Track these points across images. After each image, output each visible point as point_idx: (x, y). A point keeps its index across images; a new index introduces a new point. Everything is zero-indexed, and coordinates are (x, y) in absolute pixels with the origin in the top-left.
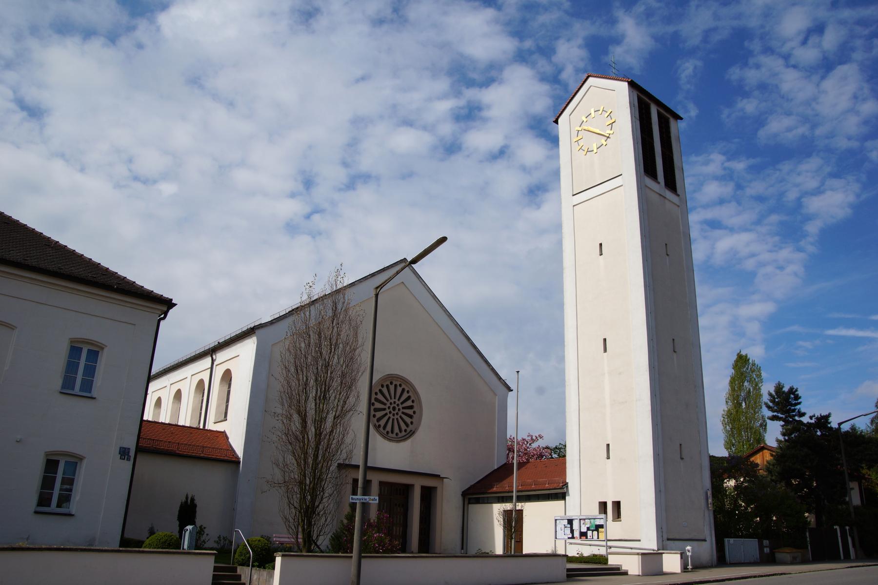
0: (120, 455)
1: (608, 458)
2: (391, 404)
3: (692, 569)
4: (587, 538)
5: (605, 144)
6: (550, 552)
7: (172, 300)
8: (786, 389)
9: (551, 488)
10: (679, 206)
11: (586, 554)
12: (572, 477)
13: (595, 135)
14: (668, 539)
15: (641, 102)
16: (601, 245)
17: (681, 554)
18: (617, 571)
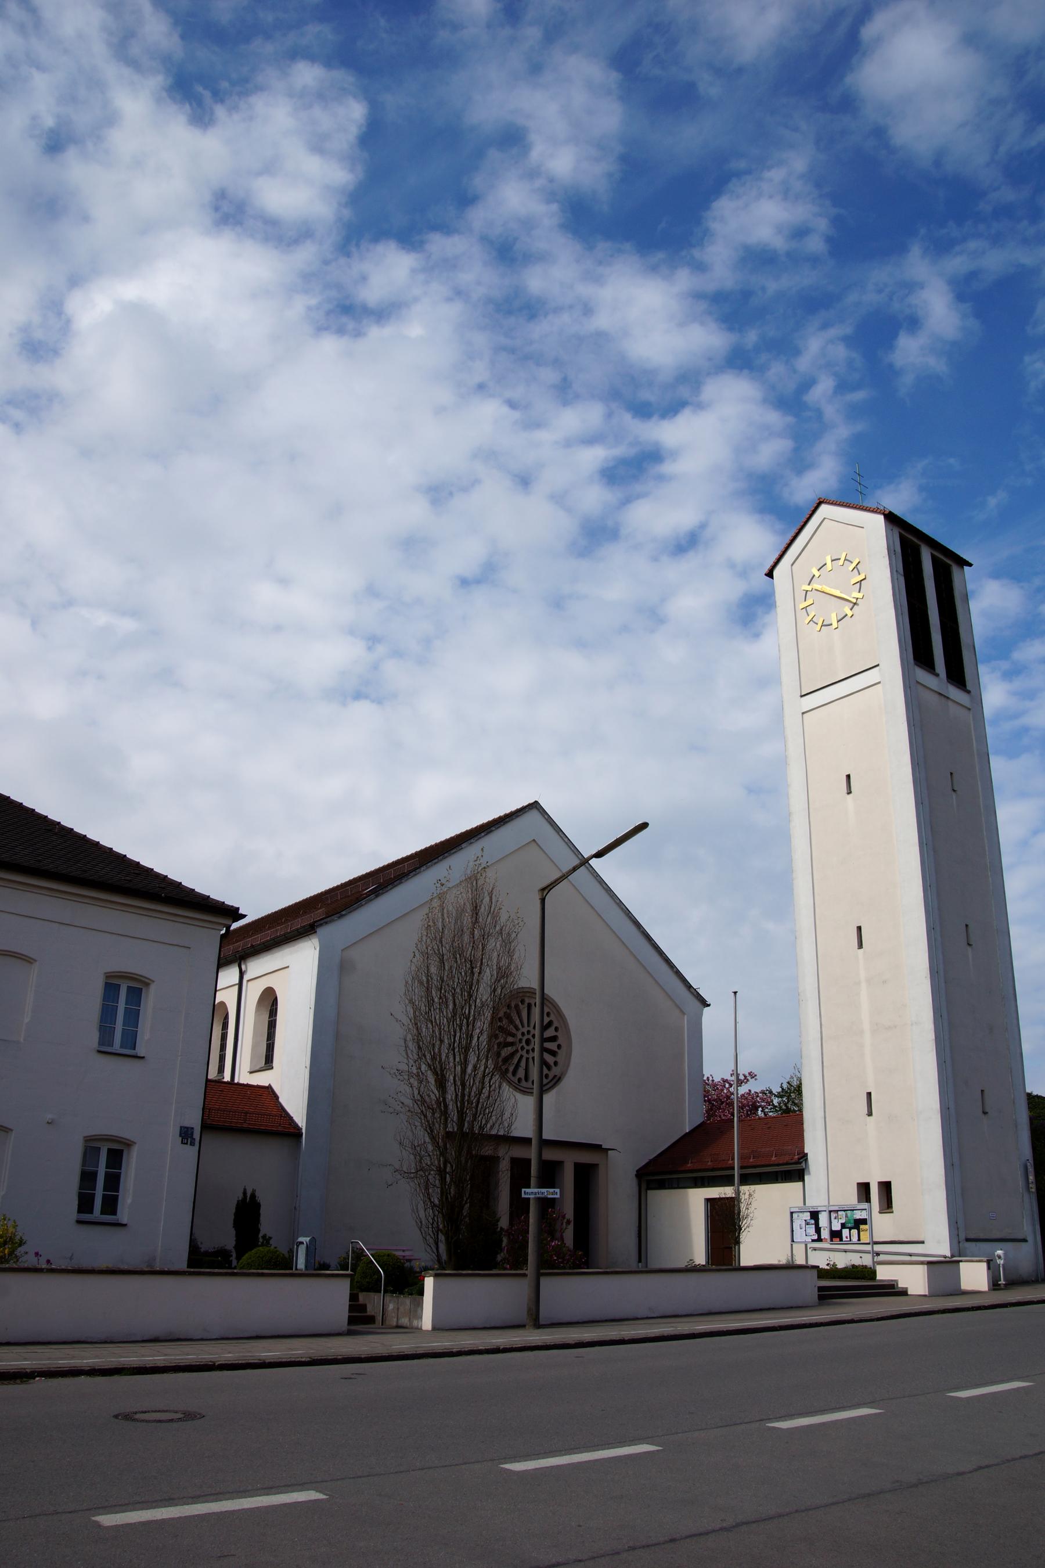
0: (181, 1138)
1: (870, 1114)
2: (523, 1034)
3: (1005, 1285)
4: (841, 1240)
5: (850, 614)
6: (783, 1262)
7: (238, 909)
9: (781, 1162)
10: (969, 709)
11: (840, 1265)
12: (813, 1144)
13: (835, 598)
14: (968, 1240)
15: (904, 542)
16: (848, 776)
17: (989, 1262)
18: (891, 1289)
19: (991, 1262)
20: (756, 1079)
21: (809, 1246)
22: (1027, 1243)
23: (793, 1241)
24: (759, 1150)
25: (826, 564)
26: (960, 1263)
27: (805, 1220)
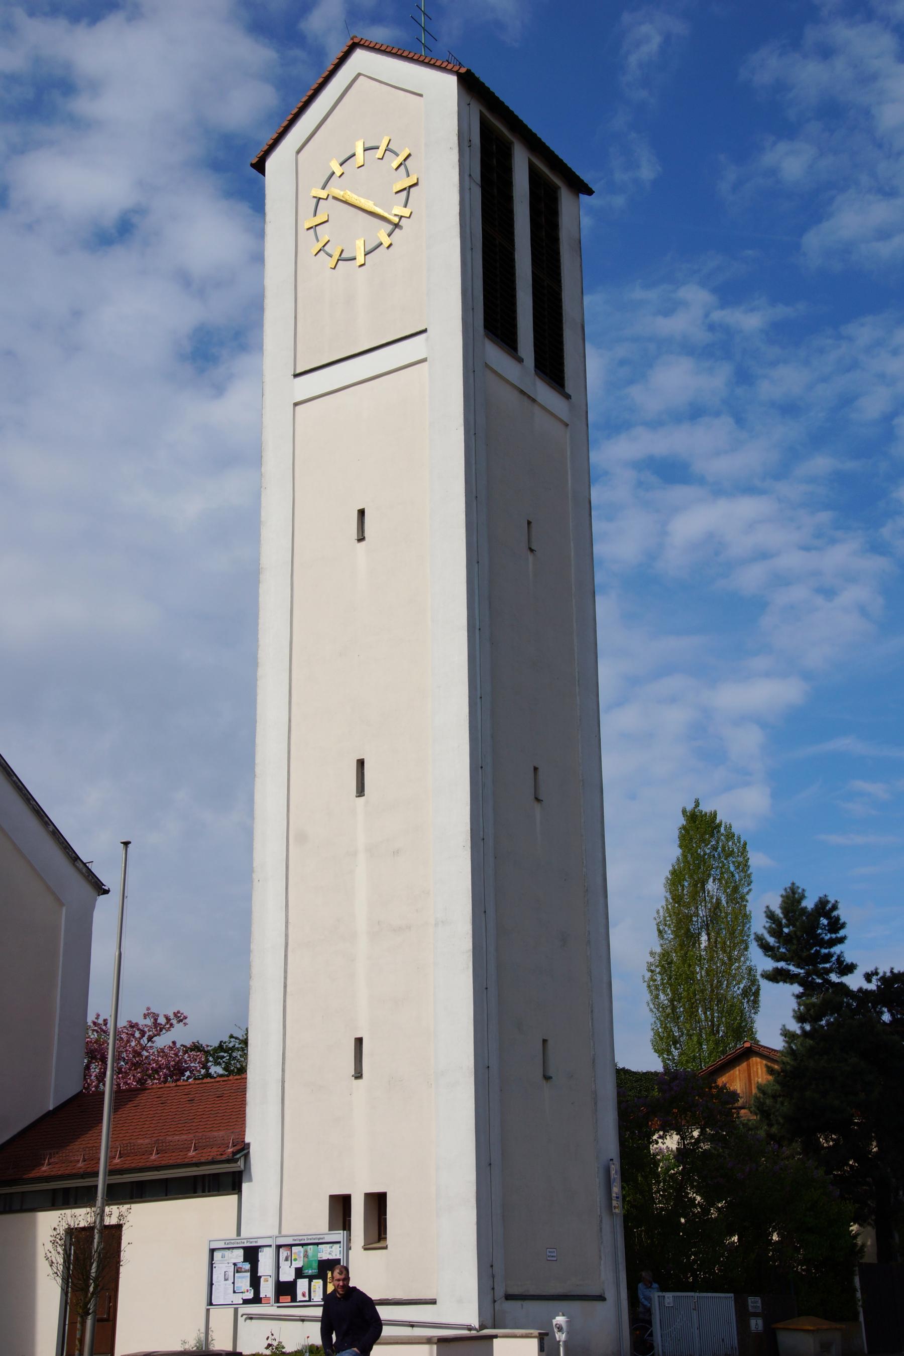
1: (358, 1075)
4: (294, 1299)
8: (809, 904)
9: (203, 1160)
10: (567, 425)
14: (509, 1297)
16: (362, 513)
17: (542, 1338)
19: (546, 1338)
20: (185, 1024)
21: (241, 1311)
22: (604, 1303)
23: (210, 1303)
24: (169, 1138)
25: (354, 155)
26: (494, 1340)
27: (235, 1264)
